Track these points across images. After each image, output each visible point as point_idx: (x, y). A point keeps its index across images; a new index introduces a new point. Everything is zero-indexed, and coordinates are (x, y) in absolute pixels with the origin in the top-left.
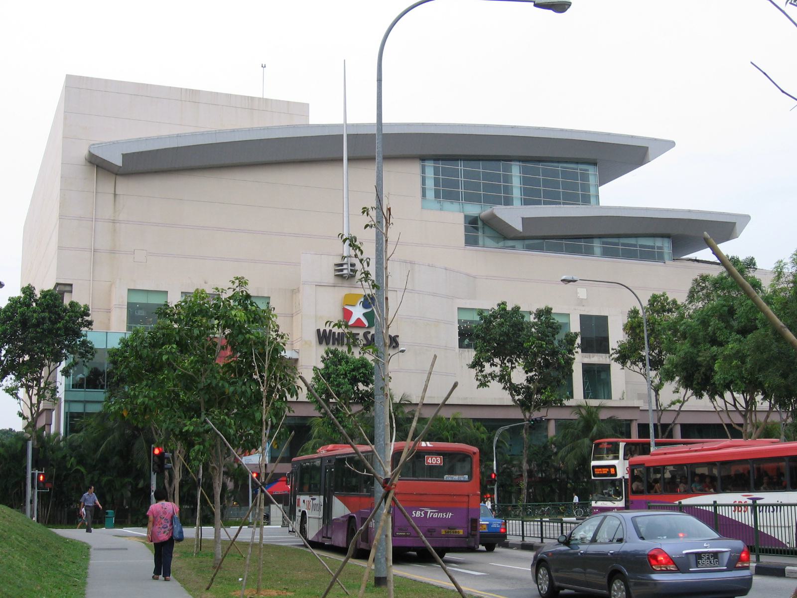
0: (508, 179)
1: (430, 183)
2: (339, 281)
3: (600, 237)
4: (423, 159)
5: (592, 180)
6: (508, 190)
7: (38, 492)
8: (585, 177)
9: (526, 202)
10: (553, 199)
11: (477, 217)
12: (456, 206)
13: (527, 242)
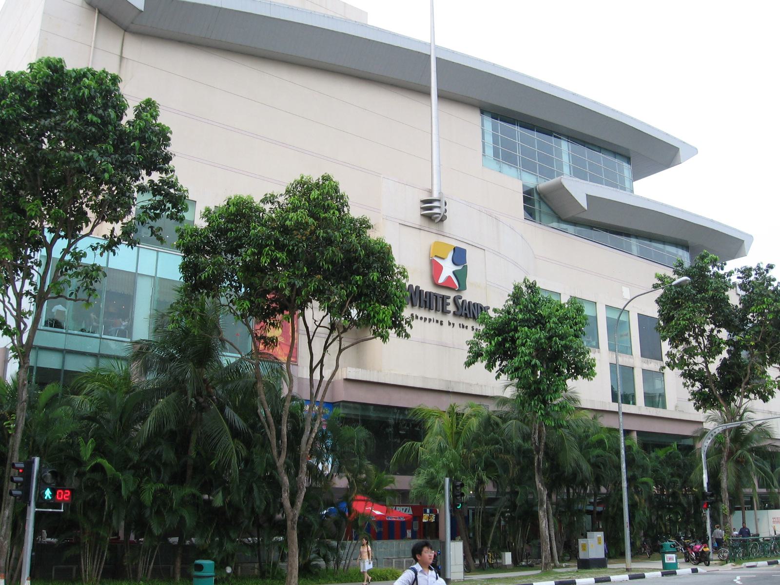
2: (425, 223)
7: (37, 513)
11: (533, 189)
12: (513, 171)
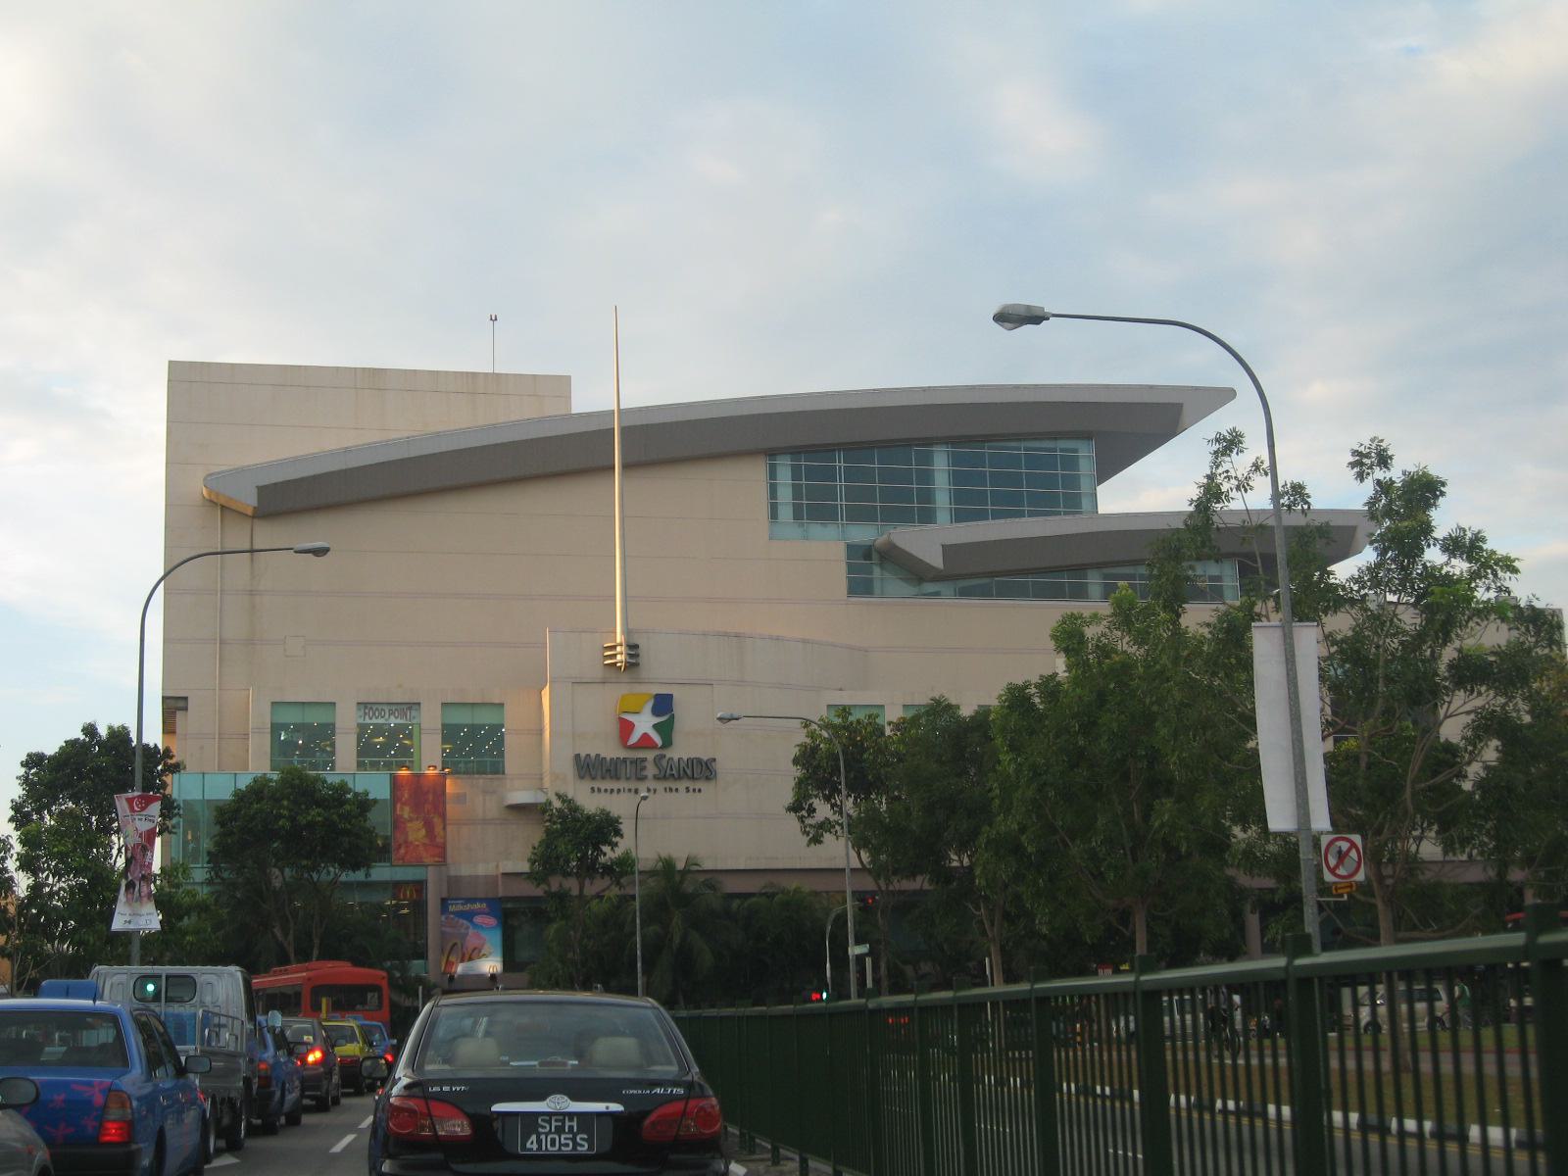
0: (927, 477)
1: (785, 495)
3: (1098, 566)
4: (772, 453)
5: (1086, 467)
6: (927, 496)
8: (1071, 463)
9: (959, 516)
10: (1010, 506)
13: (1106, 571)
